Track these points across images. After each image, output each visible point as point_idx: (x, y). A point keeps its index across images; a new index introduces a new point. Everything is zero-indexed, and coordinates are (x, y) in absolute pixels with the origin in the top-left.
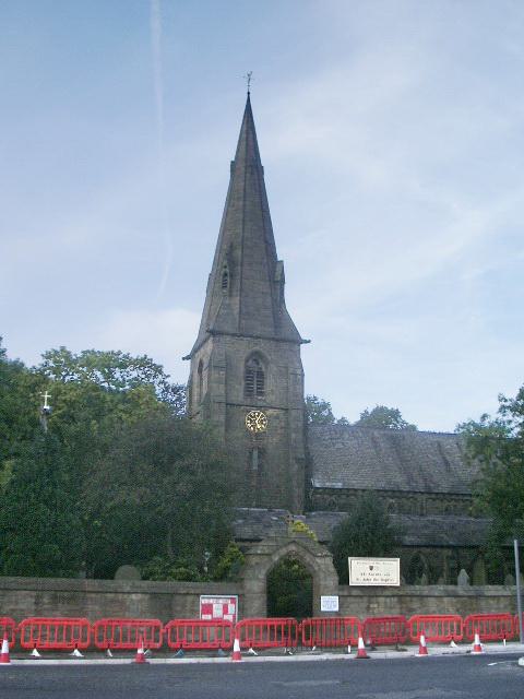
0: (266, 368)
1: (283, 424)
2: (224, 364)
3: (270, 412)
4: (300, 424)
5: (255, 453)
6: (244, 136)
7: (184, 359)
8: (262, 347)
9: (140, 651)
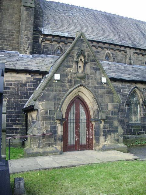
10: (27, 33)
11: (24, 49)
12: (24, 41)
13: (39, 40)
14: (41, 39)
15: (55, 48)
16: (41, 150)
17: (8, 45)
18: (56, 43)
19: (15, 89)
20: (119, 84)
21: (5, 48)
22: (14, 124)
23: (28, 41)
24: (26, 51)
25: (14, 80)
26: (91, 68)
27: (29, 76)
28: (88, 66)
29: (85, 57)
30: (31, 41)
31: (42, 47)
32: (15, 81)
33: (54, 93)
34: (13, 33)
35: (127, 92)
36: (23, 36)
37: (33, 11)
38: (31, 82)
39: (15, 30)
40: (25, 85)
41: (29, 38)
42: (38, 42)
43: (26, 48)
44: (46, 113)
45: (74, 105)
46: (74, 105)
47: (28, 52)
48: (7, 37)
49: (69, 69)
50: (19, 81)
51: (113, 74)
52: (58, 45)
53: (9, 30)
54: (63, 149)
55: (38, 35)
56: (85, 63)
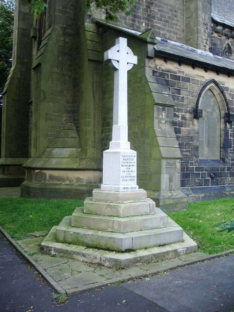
11: (203, 42)
16: (134, 184)
17: (170, 32)
21: (167, 36)
23: (207, 31)
24: (205, 46)
36: (200, 20)
39: (179, 8)
41: (207, 25)
47: (207, 48)
48: (169, 17)
51: (189, 71)
53: (171, 6)
54: (30, 114)
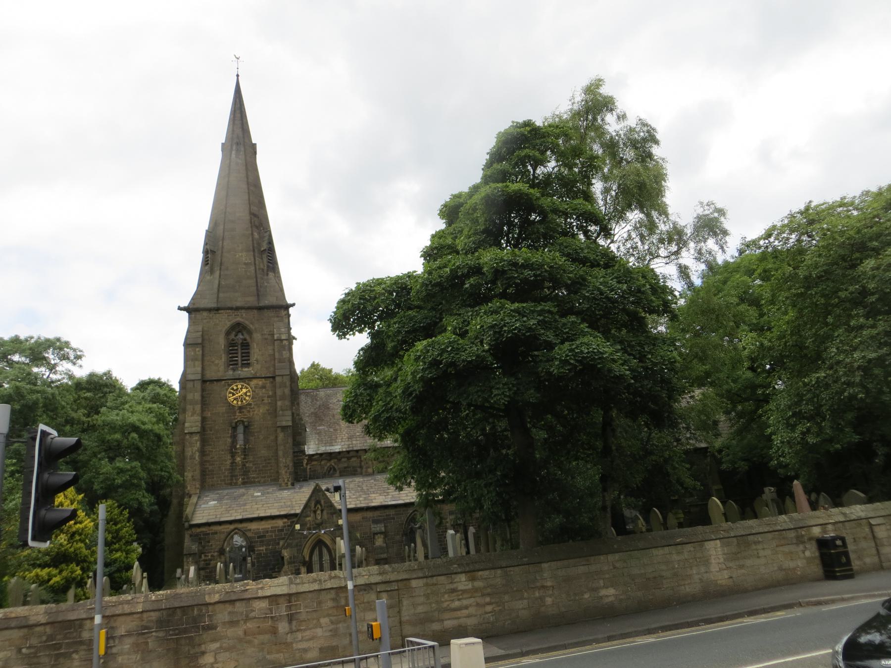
0: (251, 338)
1: (270, 393)
2: (200, 341)
3: (254, 382)
4: (287, 391)
5: (240, 429)
6: (232, 116)
7: (180, 309)
8: (242, 317)
9: (286, 554)
10: (286, 459)
11: (284, 481)
12: (283, 471)
13: (302, 462)
14: (305, 462)
15: (326, 468)
17: (265, 477)
18: (325, 461)
19: (272, 536)
20: (392, 511)
22: (273, 572)
24: (287, 483)
25: (270, 526)
26: (328, 513)
27: (285, 520)
28: (325, 512)
29: (321, 505)
30: (291, 469)
31: (308, 470)
32: (272, 528)
33: (296, 541)
34: (269, 459)
35: (404, 519)
37: (290, 431)
38: (288, 526)
40: (282, 530)
42: (303, 466)
43: (286, 480)
44: (290, 558)
45: (317, 548)
46: (317, 548)
49: (308, 519)
50: (276, 527)
52: (328, 464)
55: (301, 456)
56: (322, 511)
